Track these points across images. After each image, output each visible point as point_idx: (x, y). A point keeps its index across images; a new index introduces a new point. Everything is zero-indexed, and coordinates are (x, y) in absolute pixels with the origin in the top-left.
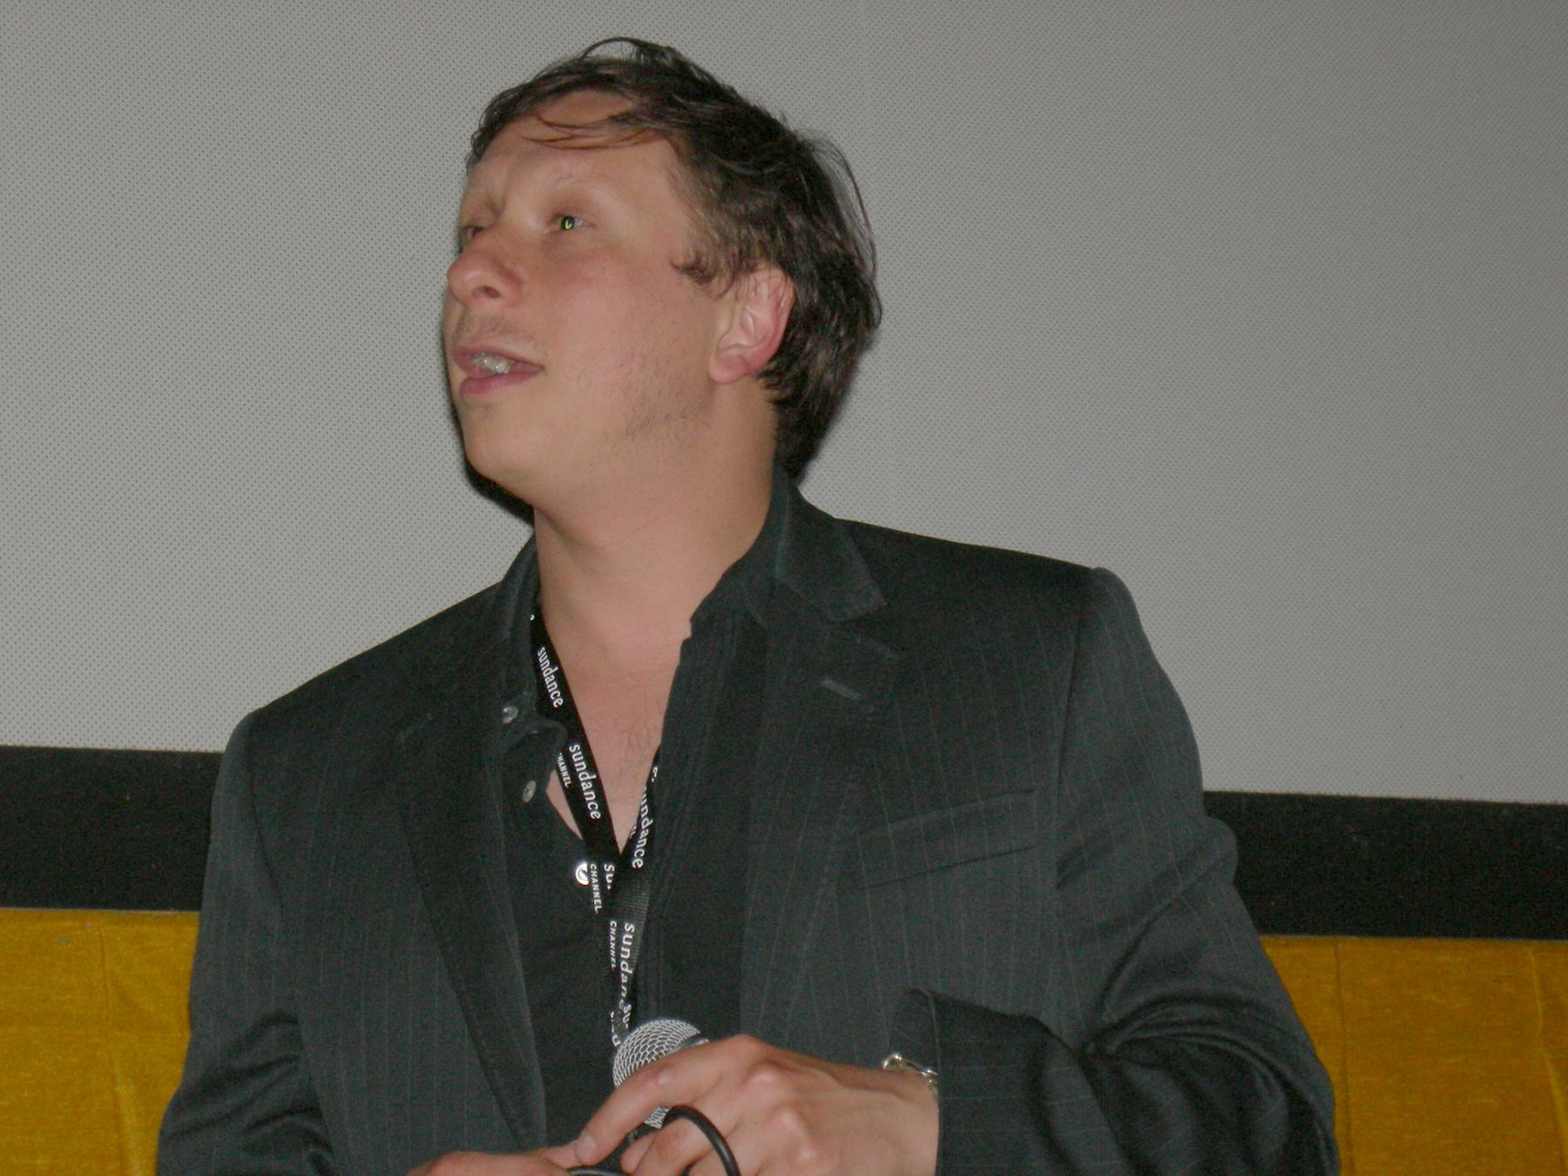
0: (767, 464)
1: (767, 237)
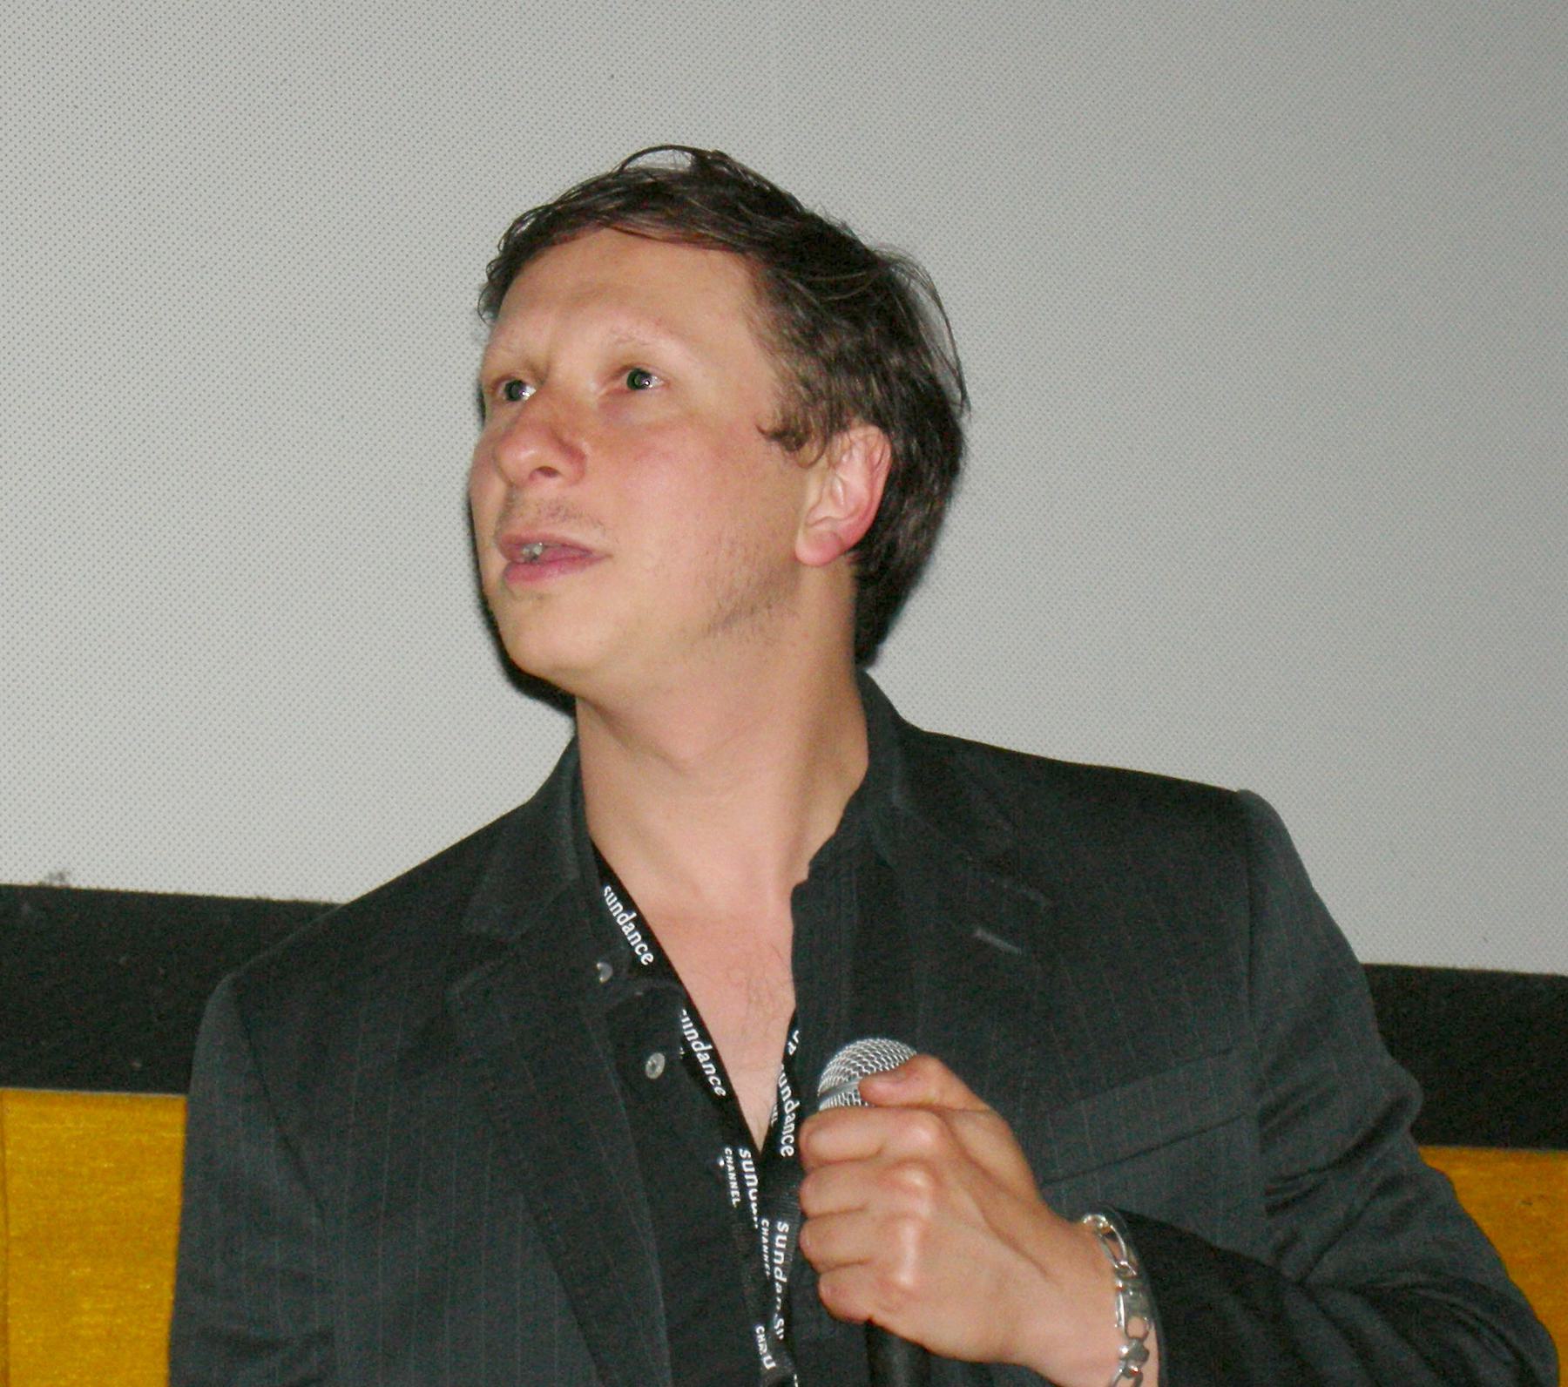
0: (852, 655)
1: (860, 388)
